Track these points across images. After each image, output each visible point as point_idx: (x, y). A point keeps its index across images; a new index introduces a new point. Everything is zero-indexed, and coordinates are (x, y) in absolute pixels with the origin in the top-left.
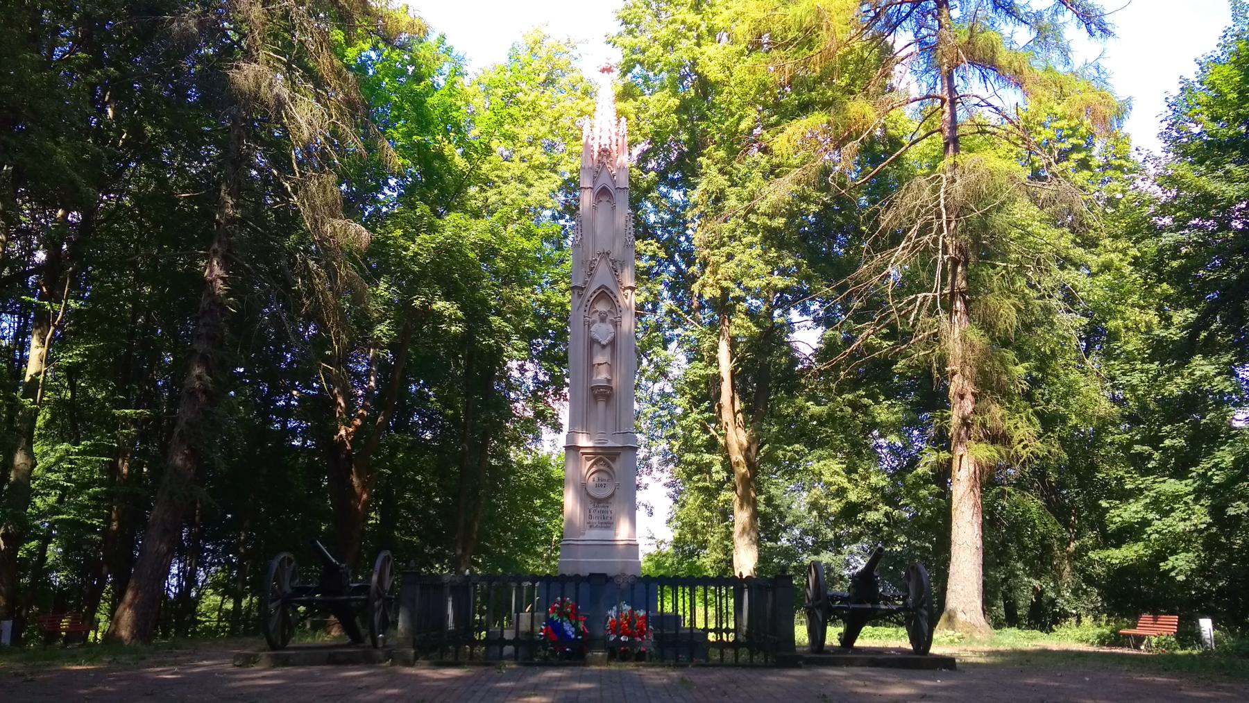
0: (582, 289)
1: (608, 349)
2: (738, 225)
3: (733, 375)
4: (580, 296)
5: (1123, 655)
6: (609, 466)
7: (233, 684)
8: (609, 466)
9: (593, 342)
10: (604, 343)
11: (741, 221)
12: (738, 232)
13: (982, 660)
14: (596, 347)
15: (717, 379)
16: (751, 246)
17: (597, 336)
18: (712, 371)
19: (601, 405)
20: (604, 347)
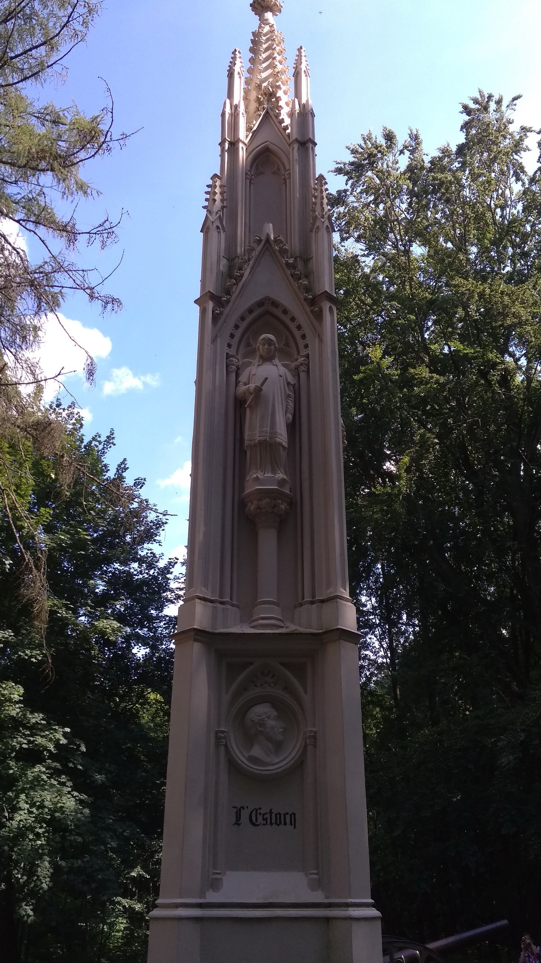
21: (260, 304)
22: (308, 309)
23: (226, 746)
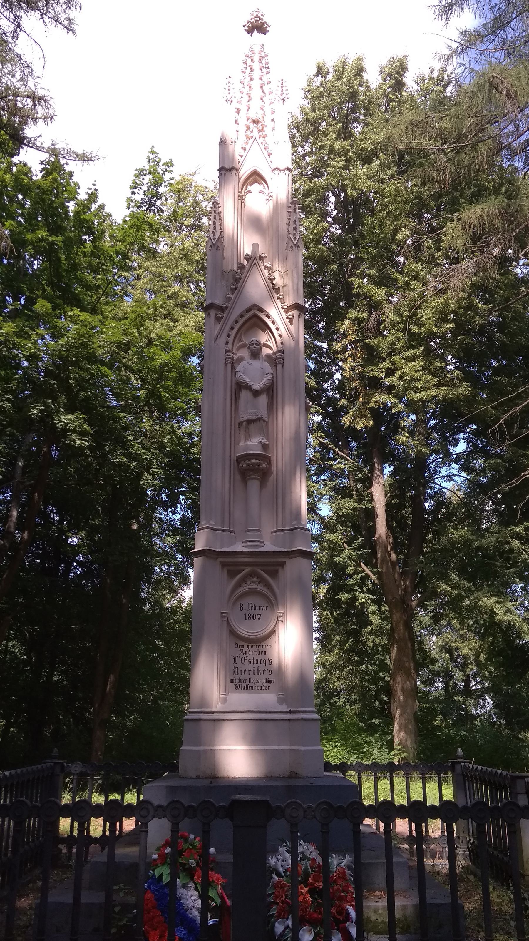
0: (222, 309)
1: (263, 399)
2: (398, 339)
3: (388, 506)
4: (218, 319)
5: (12, 844)
6: (267, 585)
7: (12, 829)
8: (267, 585)
9: (240, 387)
10: (257, 386)
11: (401, 334)
12: (399, 345)
13: (278, 784)
14: (245, 395)
15: (371, 514)
16: (413, 359)
17: (246, 378)
18: (365, 505)
19: (254, 485)
20: (256, 393)
21: (249, 310)
22: (284, 315)
23: (228, 622)
